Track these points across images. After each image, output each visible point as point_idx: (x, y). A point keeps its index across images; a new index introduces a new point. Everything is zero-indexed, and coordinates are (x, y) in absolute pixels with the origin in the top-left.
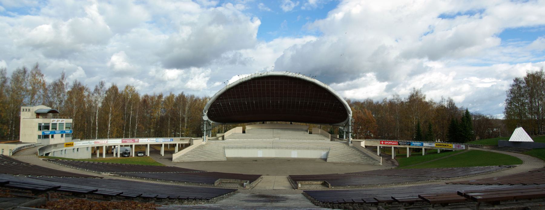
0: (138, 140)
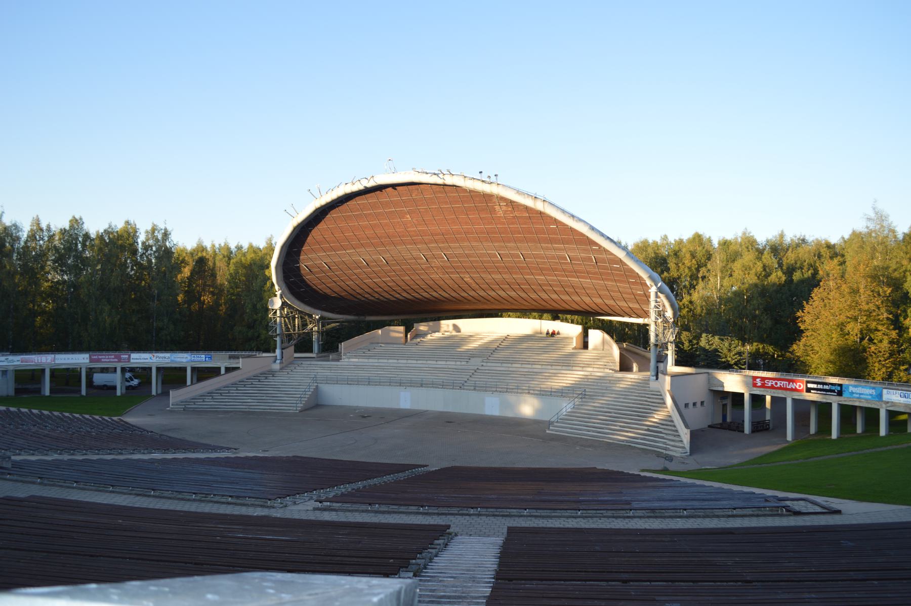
0: (130, 356)
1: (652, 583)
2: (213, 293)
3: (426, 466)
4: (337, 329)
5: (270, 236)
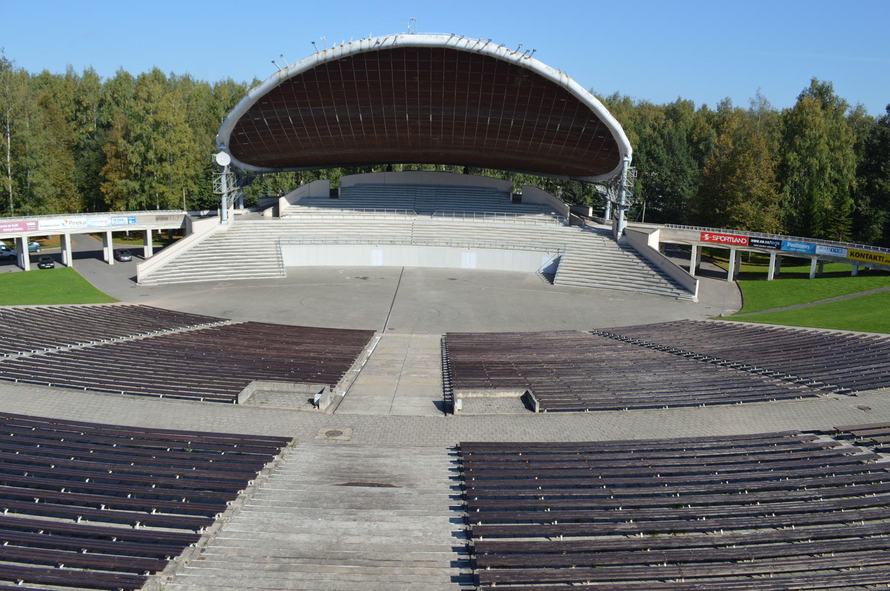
0: (37, 223)
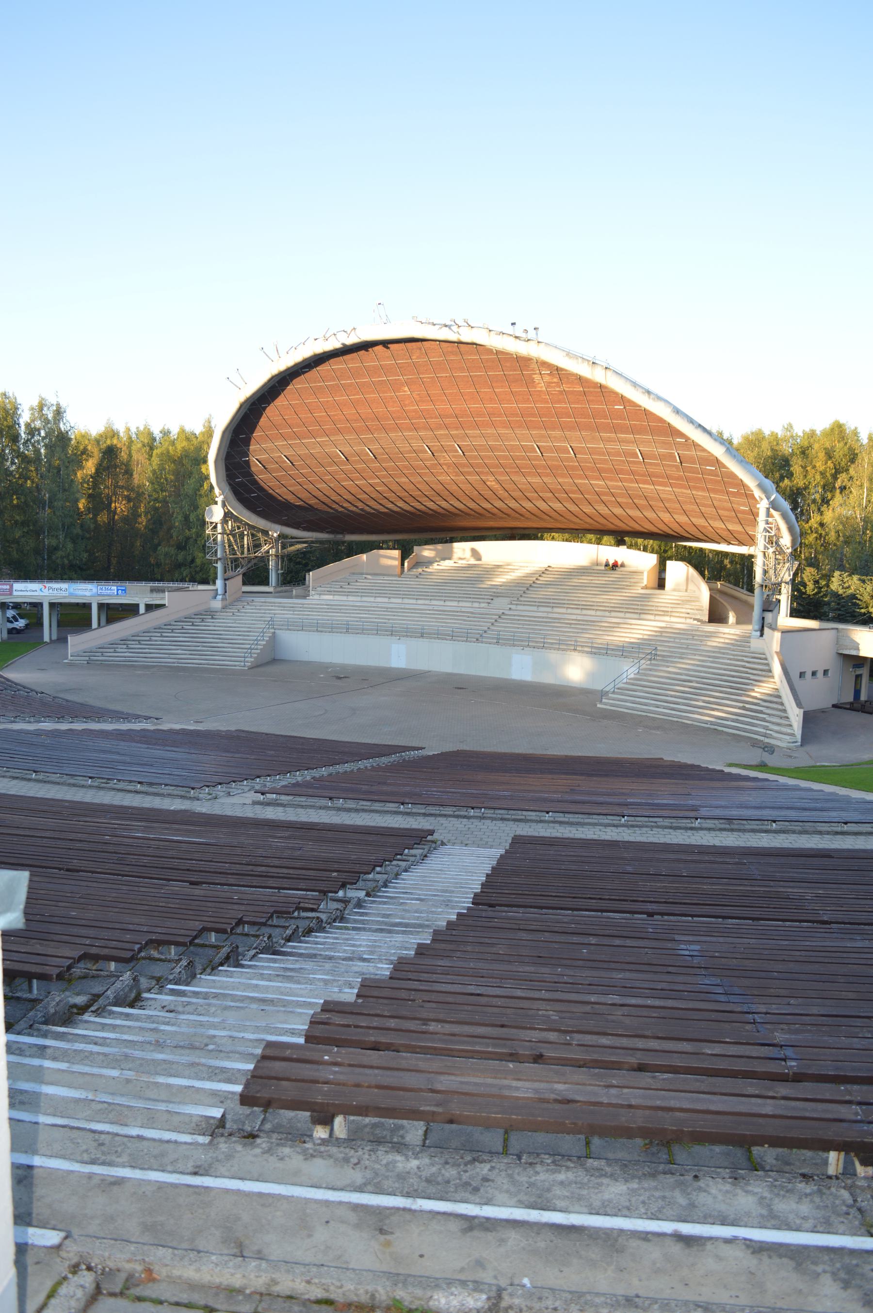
0: (12, 586)
1: (695, 919)
2: (129, 499)
3: (421, 748)
4: (304, 553)
5: (208, 416)
